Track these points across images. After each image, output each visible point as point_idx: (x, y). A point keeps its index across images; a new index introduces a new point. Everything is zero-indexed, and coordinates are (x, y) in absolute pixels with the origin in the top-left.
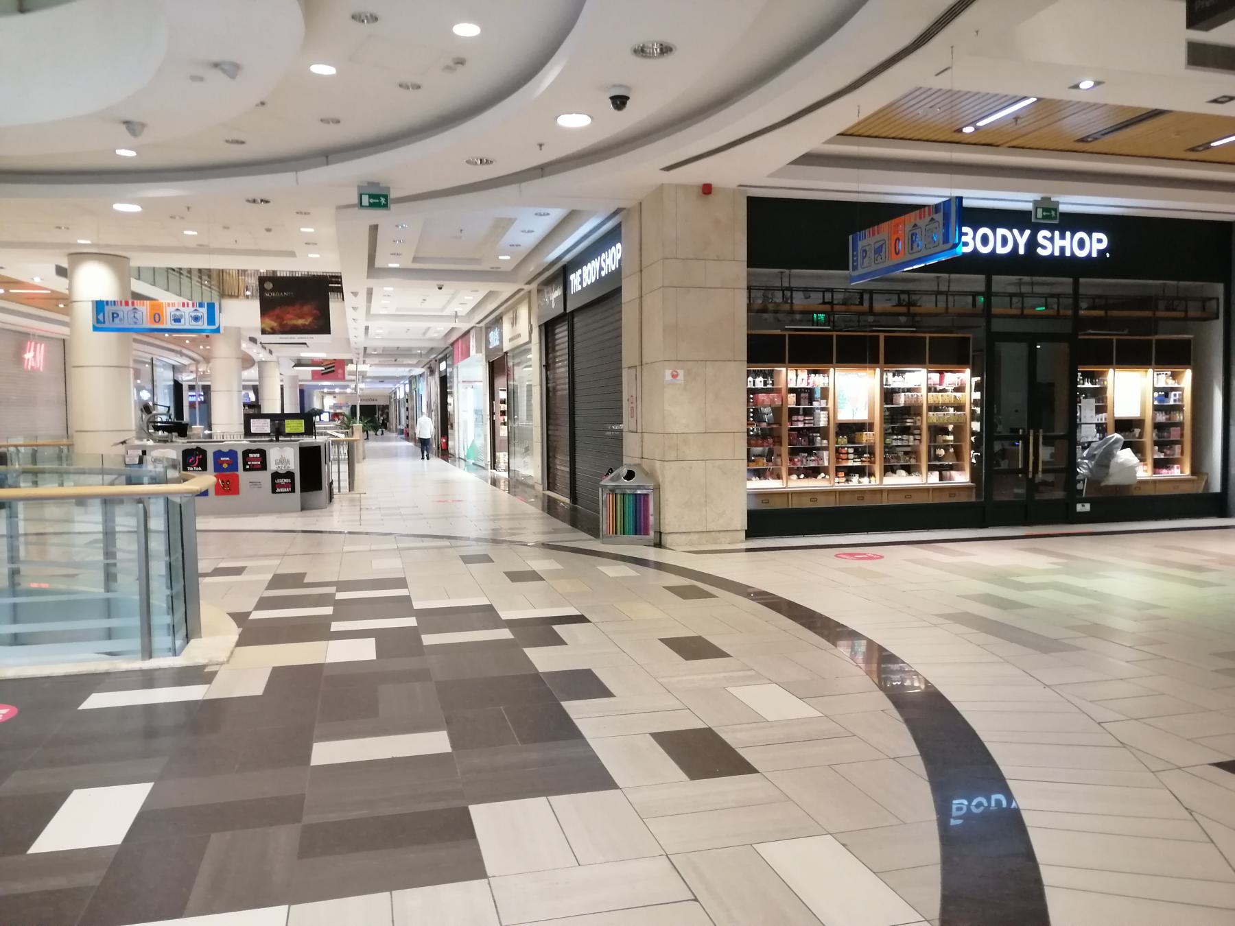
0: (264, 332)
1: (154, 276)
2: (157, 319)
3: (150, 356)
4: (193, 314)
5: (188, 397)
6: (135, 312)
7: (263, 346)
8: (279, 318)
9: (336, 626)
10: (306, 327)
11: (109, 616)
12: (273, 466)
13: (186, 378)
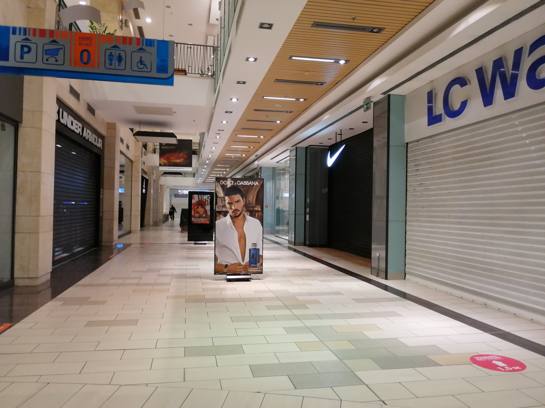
2: (85, 59)
8: (168, 159)
10: (181, 163)
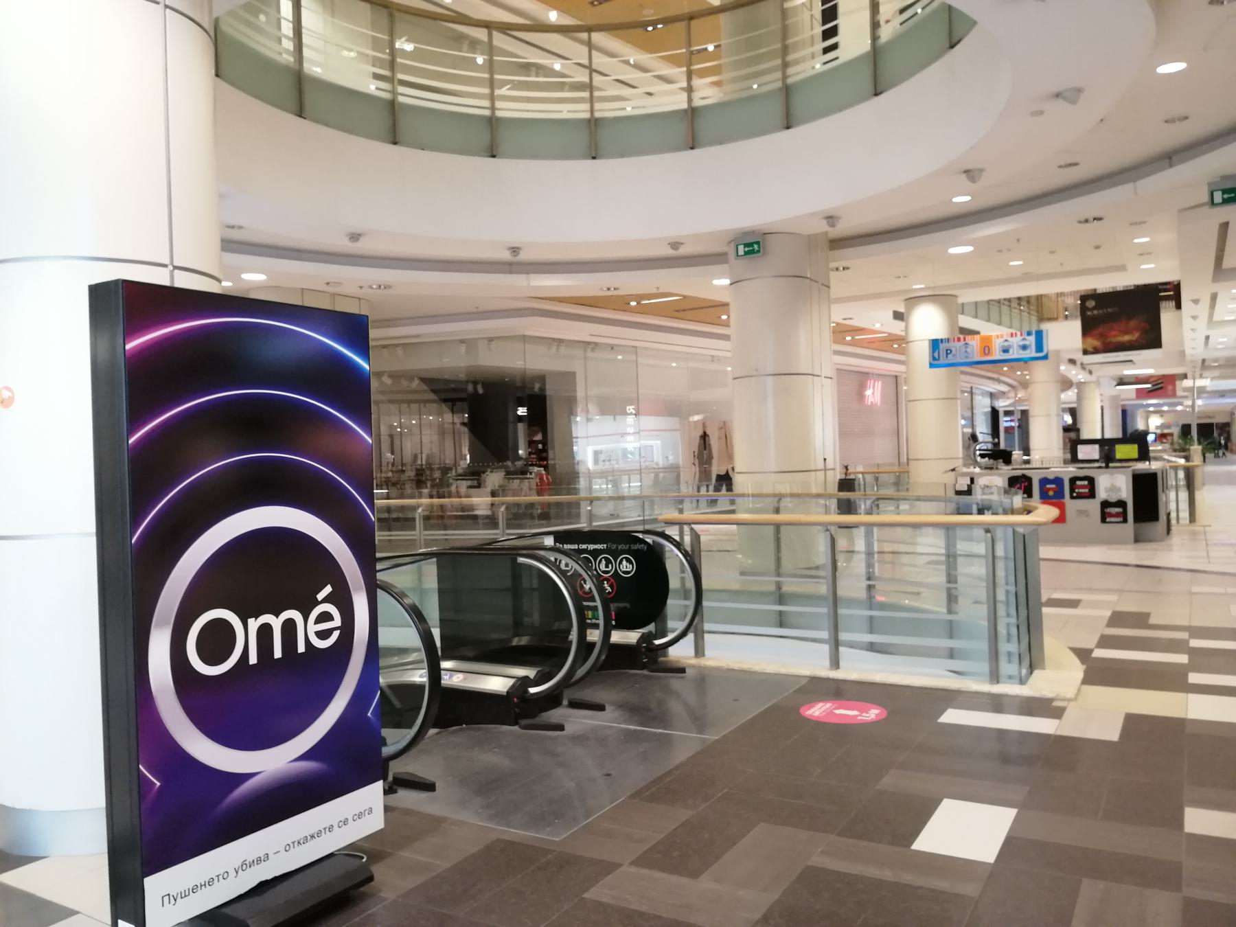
0: (1085, 352)
1: (977, 309)
3: (969, 385)
4: (1021, 343)
5: (1004, 422)
6: (966, 347)
7: (1083, 366)
8: (1102, 336)
9: (1194, 678)
11: (951, 637)
12: (1102, 494)
13: (1002, 404)
